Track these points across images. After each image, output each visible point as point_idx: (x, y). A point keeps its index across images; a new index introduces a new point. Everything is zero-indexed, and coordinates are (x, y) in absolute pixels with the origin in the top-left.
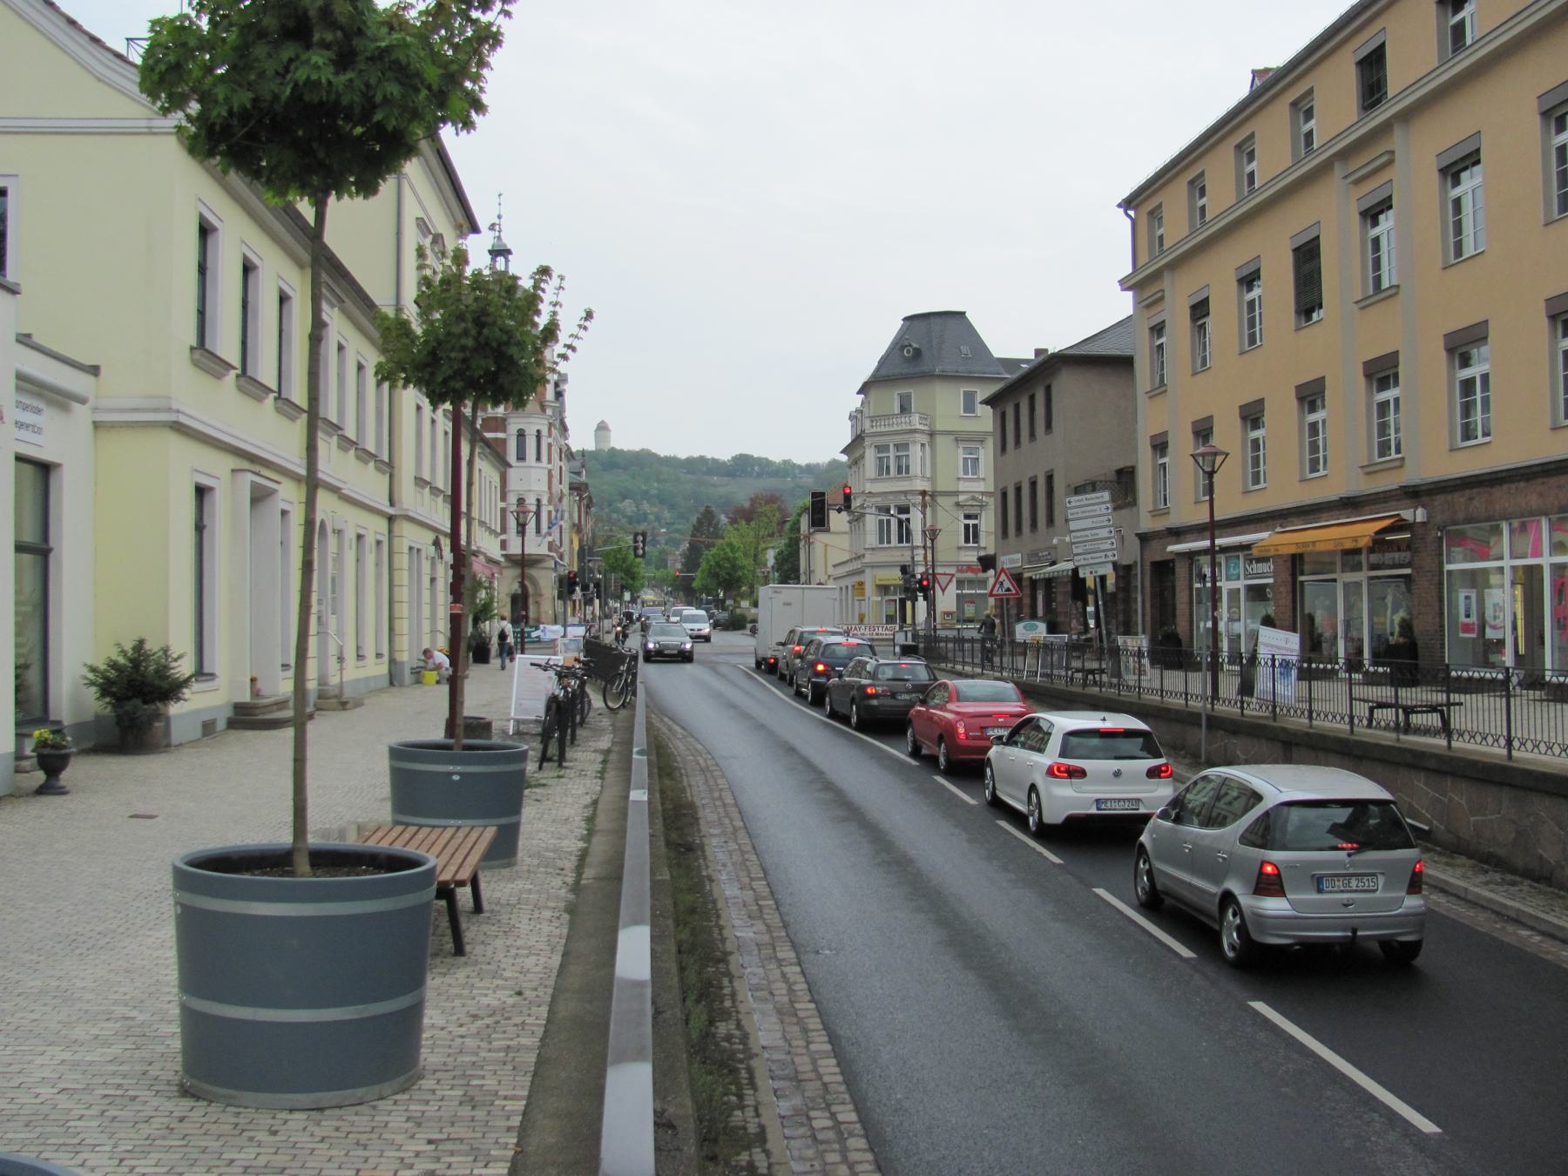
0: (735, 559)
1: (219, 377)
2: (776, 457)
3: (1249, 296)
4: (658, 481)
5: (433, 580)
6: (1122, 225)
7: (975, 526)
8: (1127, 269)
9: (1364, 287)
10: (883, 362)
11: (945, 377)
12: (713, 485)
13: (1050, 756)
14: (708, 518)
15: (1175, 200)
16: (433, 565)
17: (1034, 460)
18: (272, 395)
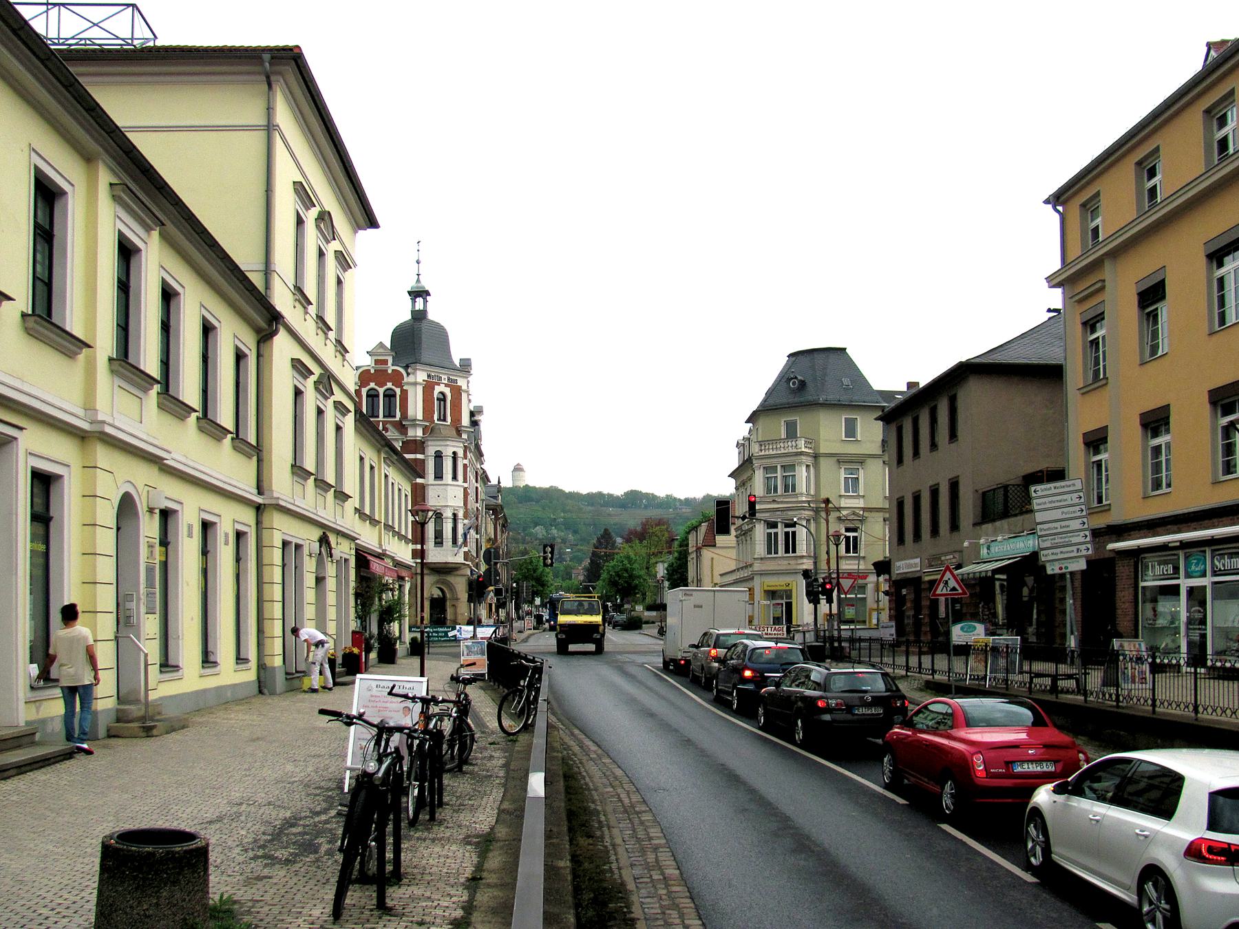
0: (633, 569)
1: (219, 440)
2: (661, 493)
3: (1220, 273)
4: (564, 511)
5: (320, 580)
6: (1051, 219)
7: (855, 538)
8: (1056, 265)
9: (1085, 378)
10: (770, 393)
11: (828, 405)
12: (609, 515)
13: (1188, 824)
14: (606, 538)
15: (1124, 177)
16: (320, 563)
17: (934, 469)
18: (157, 388)
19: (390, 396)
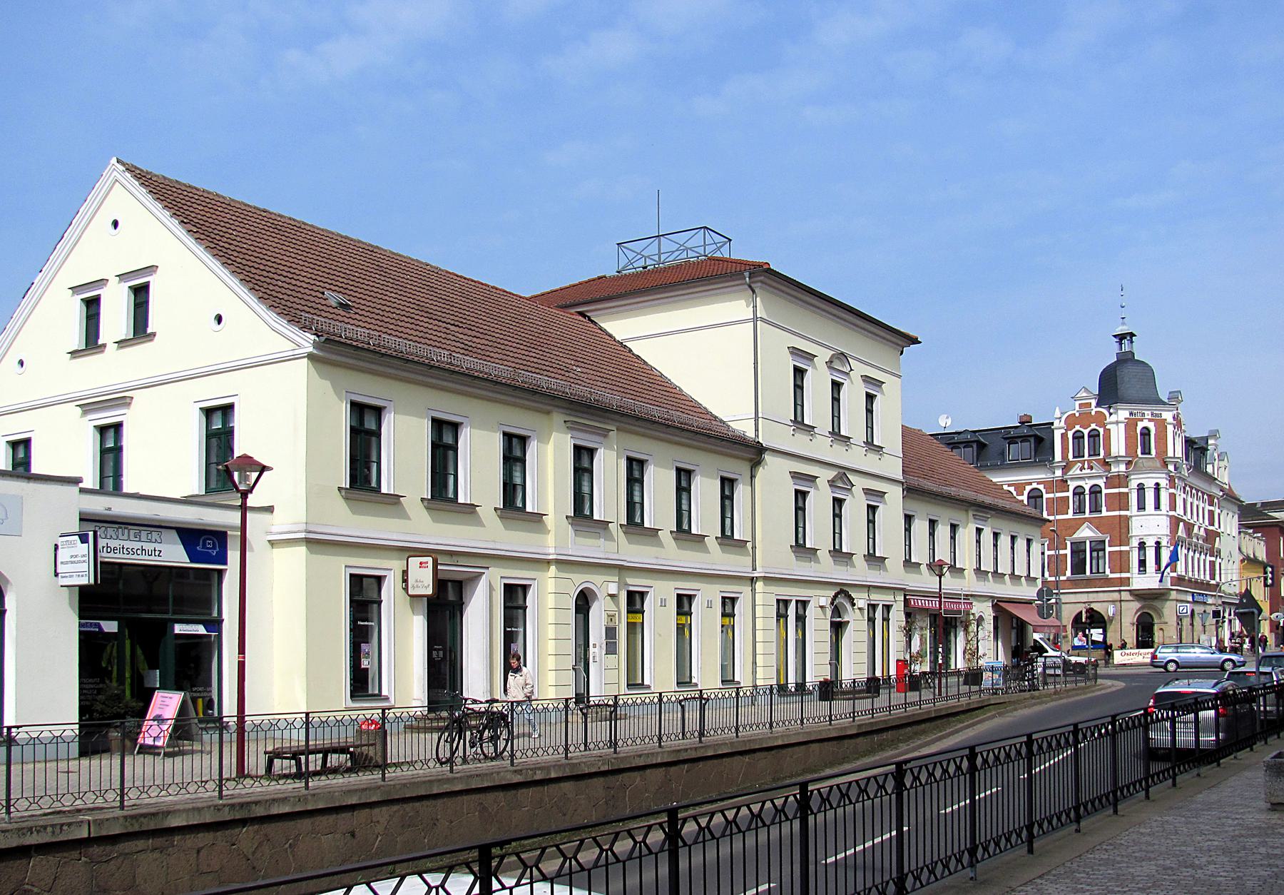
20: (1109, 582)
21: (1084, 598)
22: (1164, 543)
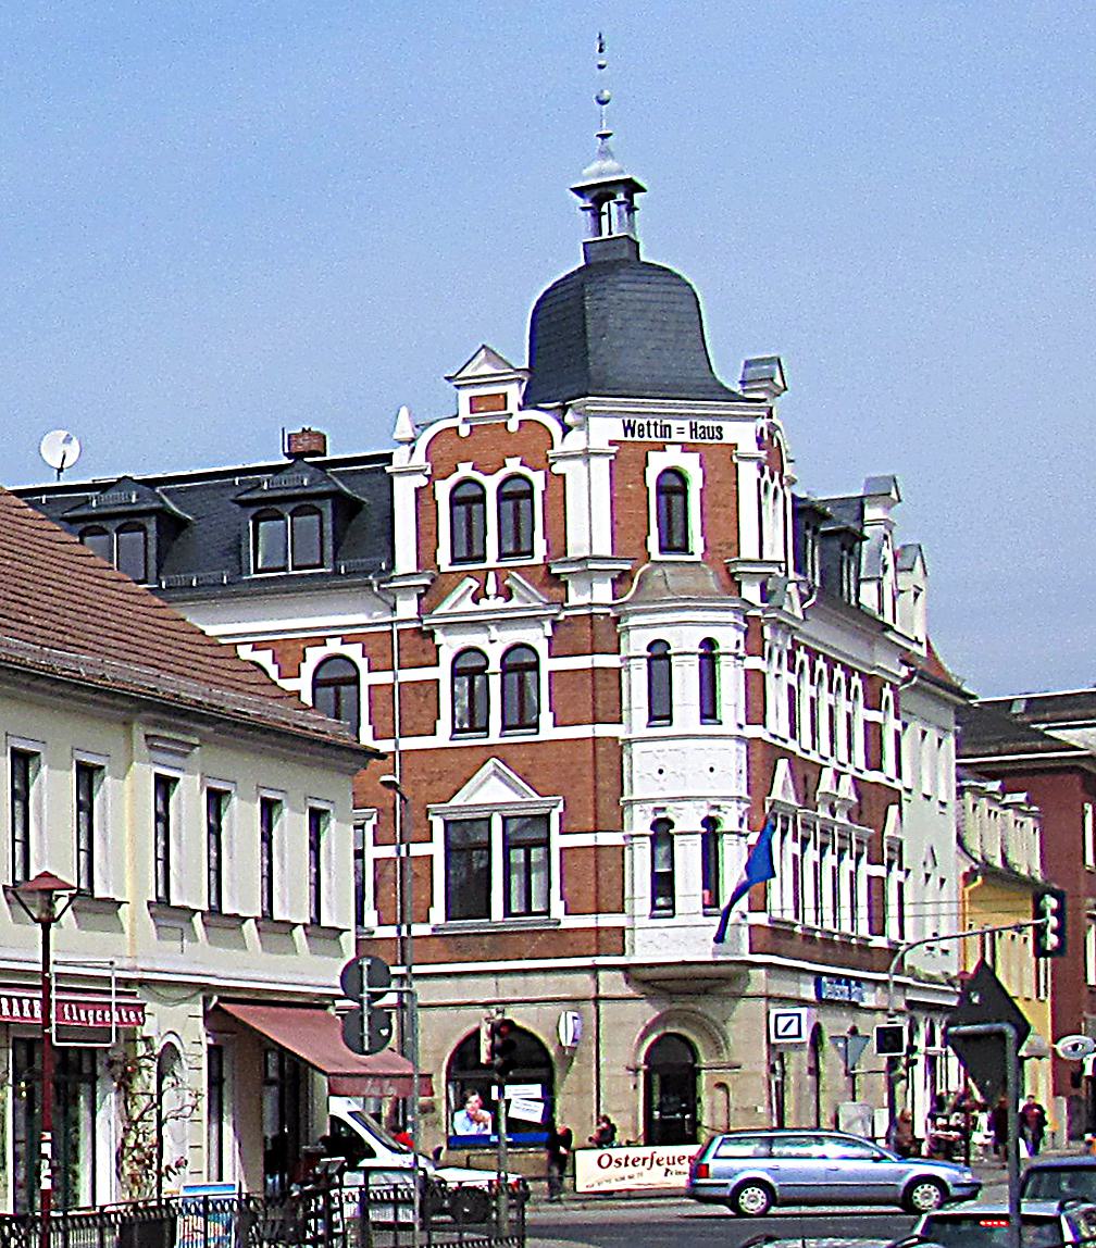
19: (515, 495)
20: (561, 941)
21: (484, 990)
22: (729, 822)
